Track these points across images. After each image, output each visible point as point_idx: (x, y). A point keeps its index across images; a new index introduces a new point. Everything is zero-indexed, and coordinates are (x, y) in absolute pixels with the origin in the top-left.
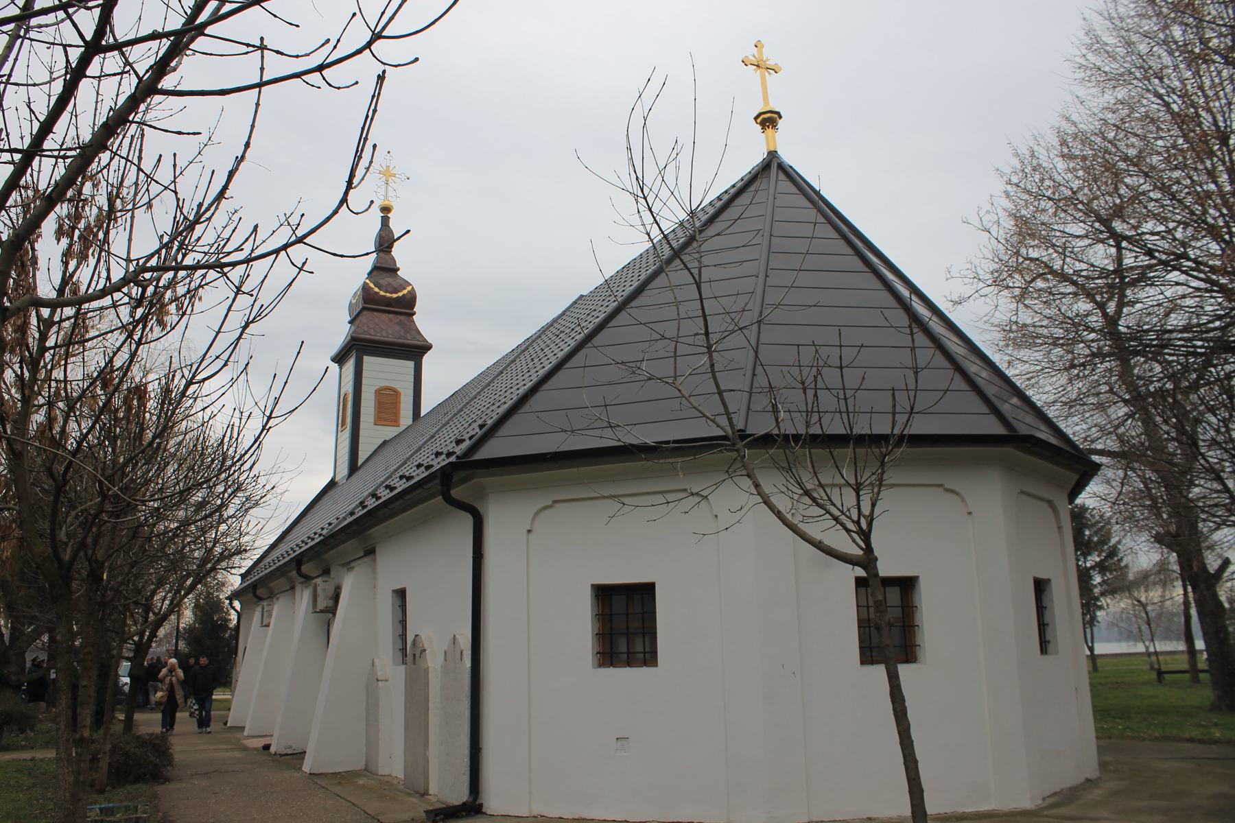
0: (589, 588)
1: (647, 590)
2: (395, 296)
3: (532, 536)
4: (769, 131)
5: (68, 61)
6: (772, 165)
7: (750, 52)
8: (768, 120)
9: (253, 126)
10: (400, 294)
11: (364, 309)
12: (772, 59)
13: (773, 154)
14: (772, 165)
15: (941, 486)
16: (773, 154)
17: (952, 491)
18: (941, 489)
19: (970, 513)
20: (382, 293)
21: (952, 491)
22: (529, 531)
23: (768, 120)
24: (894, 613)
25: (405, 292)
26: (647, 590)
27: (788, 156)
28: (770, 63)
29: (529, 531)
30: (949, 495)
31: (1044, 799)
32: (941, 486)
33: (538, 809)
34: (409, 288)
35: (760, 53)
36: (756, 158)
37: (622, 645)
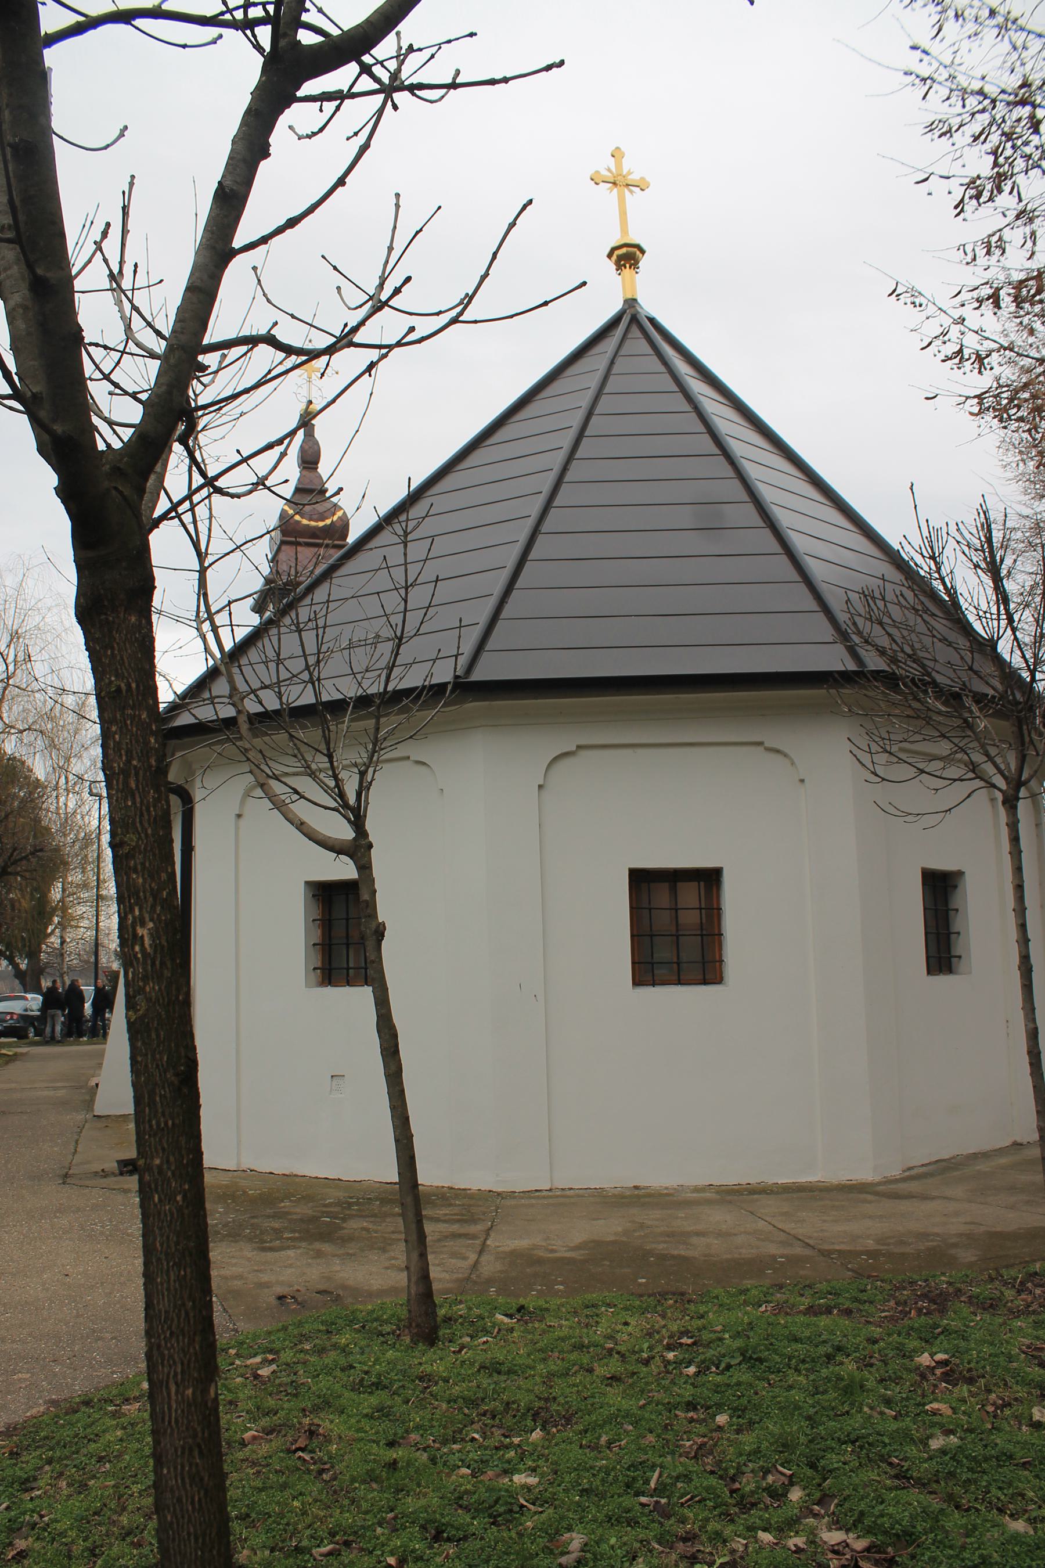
0: (301, 888)
1: (710, 879)
2: (321, 524)
3: (242, 822)
4: (627, 272)
5: (110, 270)
6: (630, 322)
7: (604, 164)
8: (627, 257)
9: (476, 322)
10: (328, 522)
11: (283, 543)
12: (634, 167)
13: (631, 303)
14: (630, 322)
15: (760, 744)
16: (631, 303)
17: (778, 751)
18: (761, 749)
19: (802, 781)
20: (305, 522)
21: (778, 751)
22: (239, 816)
23: (627, 257)
24: (690, 918)
25: (335, 518)
26: (710, 879)
27: (649, 306)
28: (634, 177)
29: (239, 816)
30: (773, 755)
31: (904, 1171)
32: (760, 744)
33: (247, 1163)
34: (340, 514)
35: (619, 165)
36: (616, 306)
37: (664, 952)
